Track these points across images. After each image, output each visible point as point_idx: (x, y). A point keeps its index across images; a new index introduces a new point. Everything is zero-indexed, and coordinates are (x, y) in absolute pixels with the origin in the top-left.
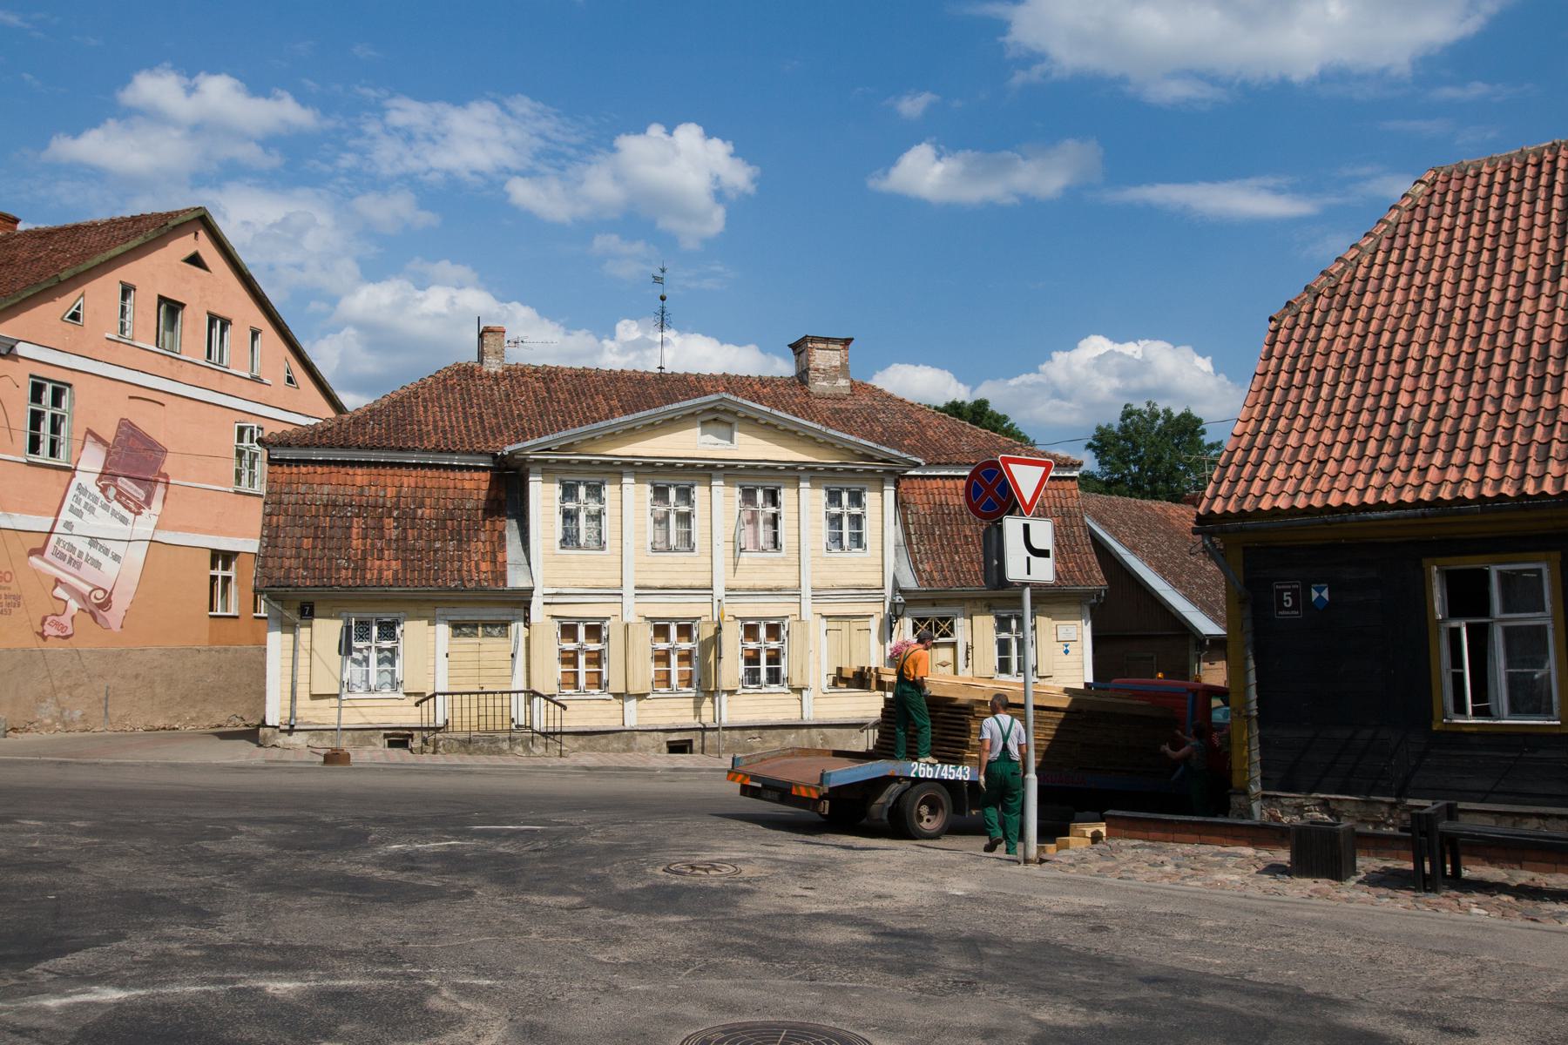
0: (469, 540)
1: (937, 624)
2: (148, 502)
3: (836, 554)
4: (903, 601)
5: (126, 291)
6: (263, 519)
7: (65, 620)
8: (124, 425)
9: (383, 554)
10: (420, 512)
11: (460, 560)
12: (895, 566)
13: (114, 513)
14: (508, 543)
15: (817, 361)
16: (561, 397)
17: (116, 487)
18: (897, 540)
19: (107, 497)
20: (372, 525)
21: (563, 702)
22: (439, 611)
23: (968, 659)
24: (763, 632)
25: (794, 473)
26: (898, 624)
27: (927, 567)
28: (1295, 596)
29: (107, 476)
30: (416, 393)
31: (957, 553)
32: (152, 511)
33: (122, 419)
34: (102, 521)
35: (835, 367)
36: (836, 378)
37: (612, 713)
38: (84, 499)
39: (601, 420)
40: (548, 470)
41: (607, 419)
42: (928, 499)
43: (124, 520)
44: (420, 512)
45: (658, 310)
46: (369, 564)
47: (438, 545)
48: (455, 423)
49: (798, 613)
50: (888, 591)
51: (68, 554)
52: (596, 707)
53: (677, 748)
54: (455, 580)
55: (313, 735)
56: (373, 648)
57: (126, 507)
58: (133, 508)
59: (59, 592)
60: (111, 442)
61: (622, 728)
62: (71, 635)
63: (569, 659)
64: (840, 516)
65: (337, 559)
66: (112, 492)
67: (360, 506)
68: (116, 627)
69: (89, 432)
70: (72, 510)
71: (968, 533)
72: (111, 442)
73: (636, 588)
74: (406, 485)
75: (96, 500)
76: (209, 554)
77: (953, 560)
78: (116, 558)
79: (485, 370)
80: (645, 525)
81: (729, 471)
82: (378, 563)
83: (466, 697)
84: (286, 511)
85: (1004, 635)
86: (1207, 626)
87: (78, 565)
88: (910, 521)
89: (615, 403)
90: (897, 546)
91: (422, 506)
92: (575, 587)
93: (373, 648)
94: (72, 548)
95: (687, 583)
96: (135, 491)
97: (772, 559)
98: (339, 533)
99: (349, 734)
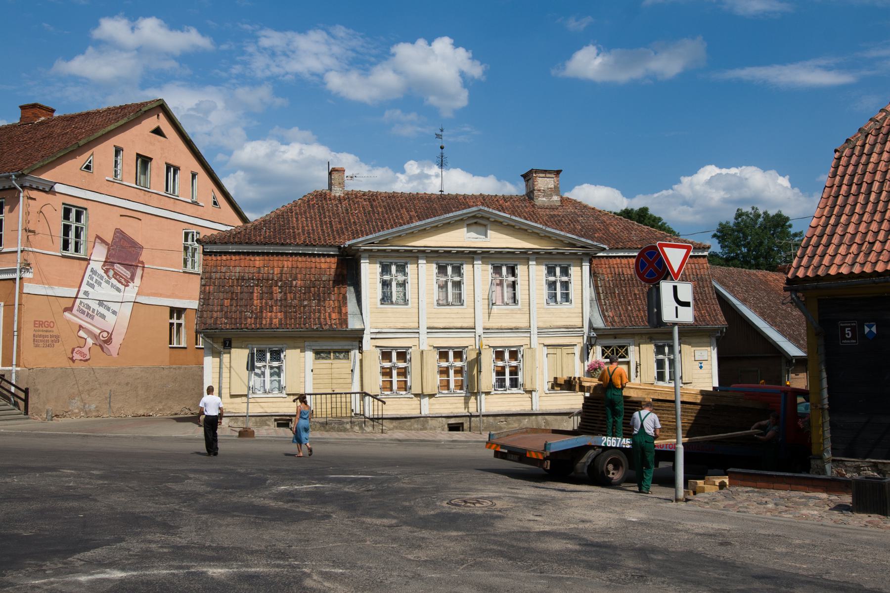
0: (325, 300)
1: (617, 350)
2: (132, 279)
3: (553, 306)
4: (595, 335)
5: (118, 151)
6: (201, 288)
7: (85, 350)
8: (118, 232)
9: (273, 309)
10: (294, 283)
11: (319, 312)
12: (590, 313)
13: (113, 286)
14: (348, 301)
15: (539, 185)
16: (380, 210)
17: (113, 269)
18: (591, 297)
19: (108, 276)
20: (266, 291)
21: (384, 400)
22: (307, 343)
23: (637, 372)
24: (507, 355)
25: (525, 256)
26: (592, 350)
27: (611, 314)
28: (853, 330)
29: (108, 263)
30: (291, 210)
31: (630, 305)
32: (135, 284)
33: (116, 229)
34: (105, 291)
35: (551, 188)
36: (551, 195)
37: (413, 406)
38: (95, 277)
39: (405, 224)
40: (373, 256)
41: (408, 223)
42: (611, 270)
43: (118, 290)
44: (294, 283)
45: (439, 154)
46: (264, 315)
47: (306, 303)
48: (315, 228)
49: (529, 343)
50: (586, 329)
51: (86, 310)
52: (404, 403)
53: (454, 428)
54: (316, 324)
55: (232, 420)
56: (267, 366)
57: (120, 282)
58: (124, 282)
59: (82, 333)
60: (110, 242)
61: (420, 415)
62: (89, 359)
63: (387, 373)
64: (555, 283)
65: (245, 312)
66: (111, 273)
67: (258, 280)
68: (115, 354)
69: (98, 237)
70: (88, 284)
71: (637, 292)
72: (110, 242)
73: (428, 328)
74: (285, 266)
75: (102, 277)
76: (168, 310)
77: (627, 309)
78: (114, 313)
79: (333, 195)
80: (433, 290)
81: (485, 255)
82: (269, 314)
83: (324, 396)
84: (214, 283)
85: (661, 357)
86: (793, 350)
87: (92, 317)
88: (600, 285)
89: (413, 213)
90: (591, 300)
91: (295, 279)
92: (390, 328)
93: (267, 366)
94: (89, 307)
95: (459, 325)
96: (125, 272)
97: (512, 310)
98: (246, 296)
99: (253, 419)
